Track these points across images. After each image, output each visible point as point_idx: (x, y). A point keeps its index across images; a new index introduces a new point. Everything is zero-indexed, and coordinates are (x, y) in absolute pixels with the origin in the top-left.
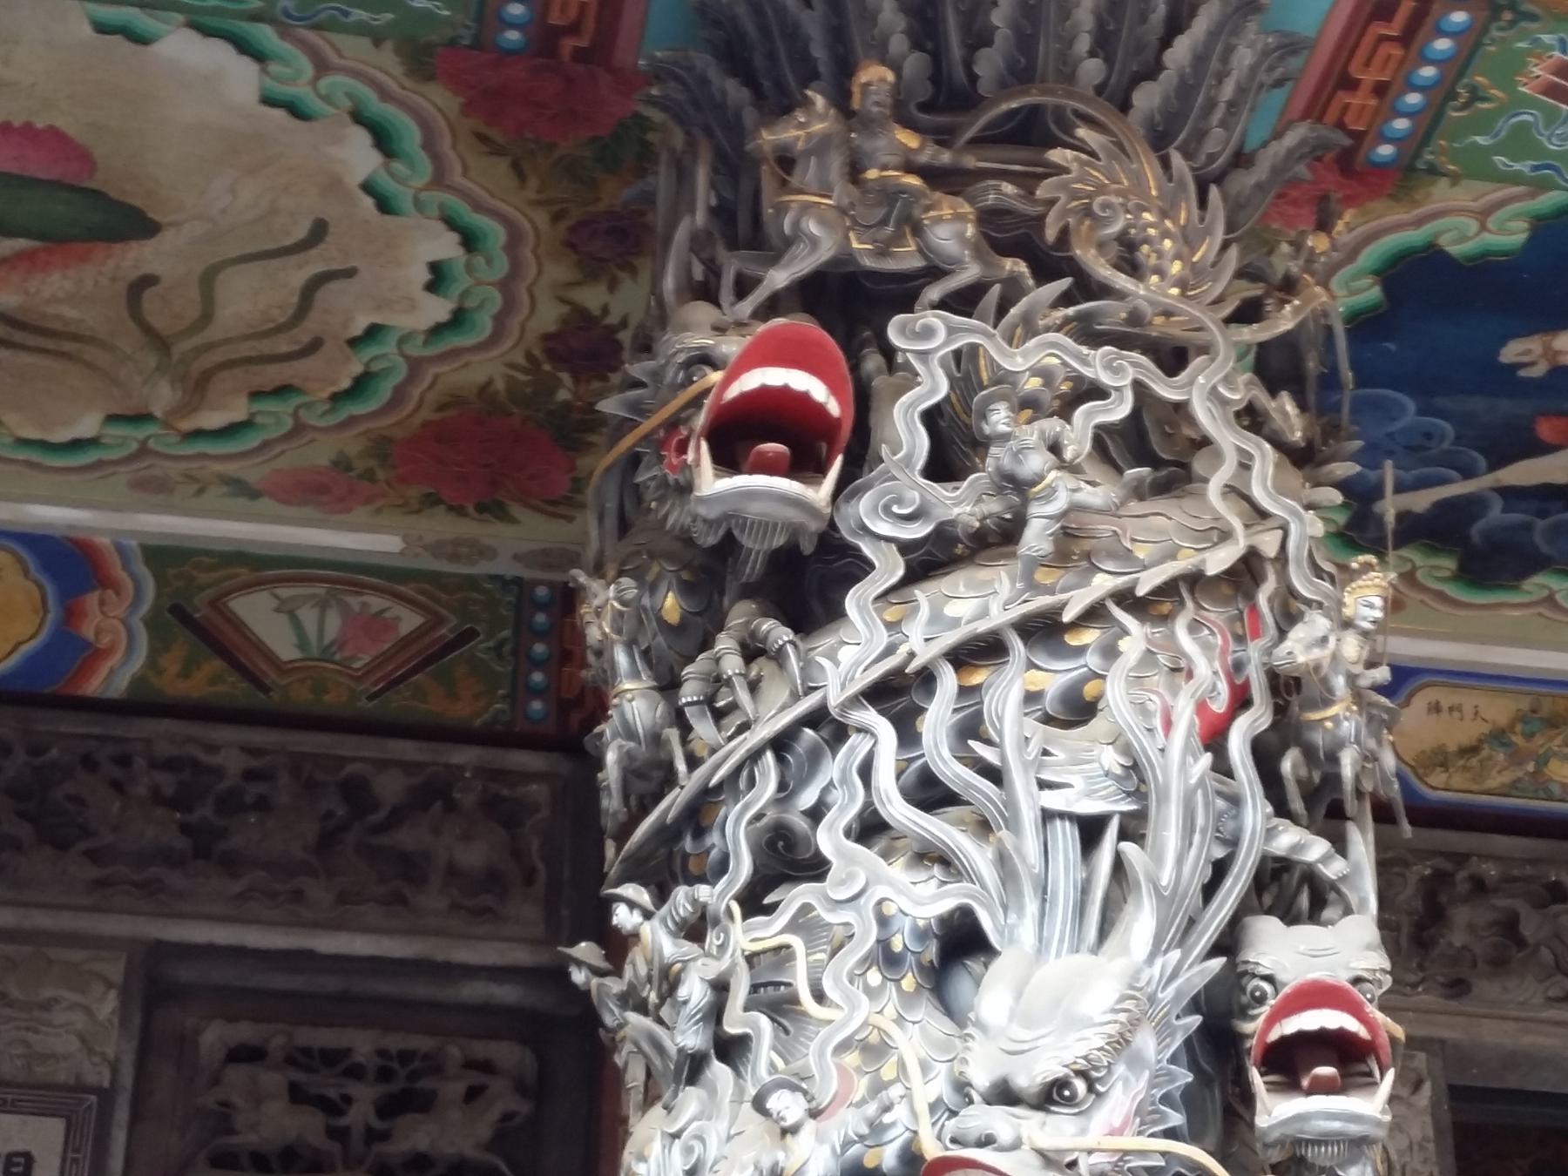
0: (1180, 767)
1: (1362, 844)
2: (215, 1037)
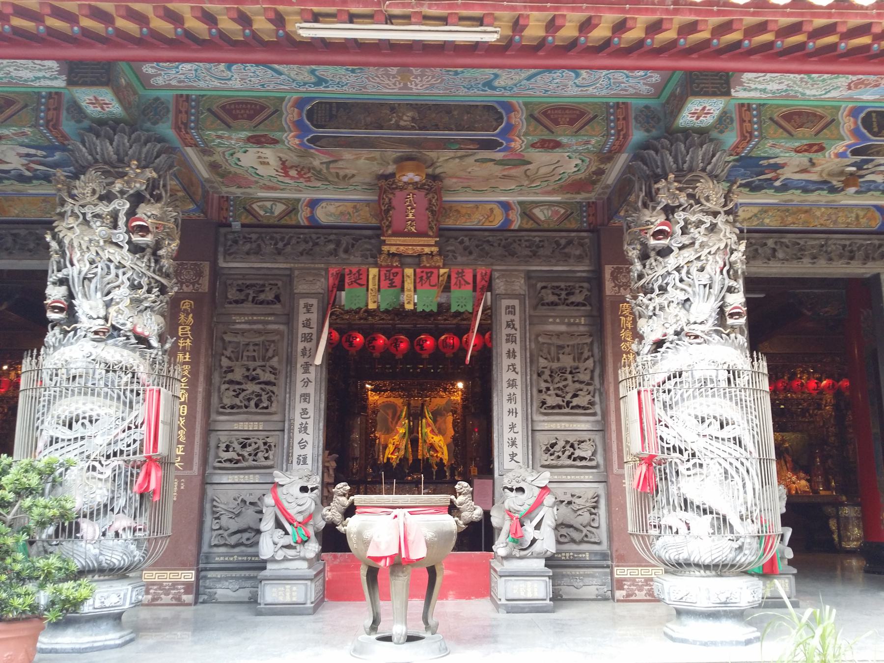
0: (718, 278)
1: (741, 281)
2: (539, 285)
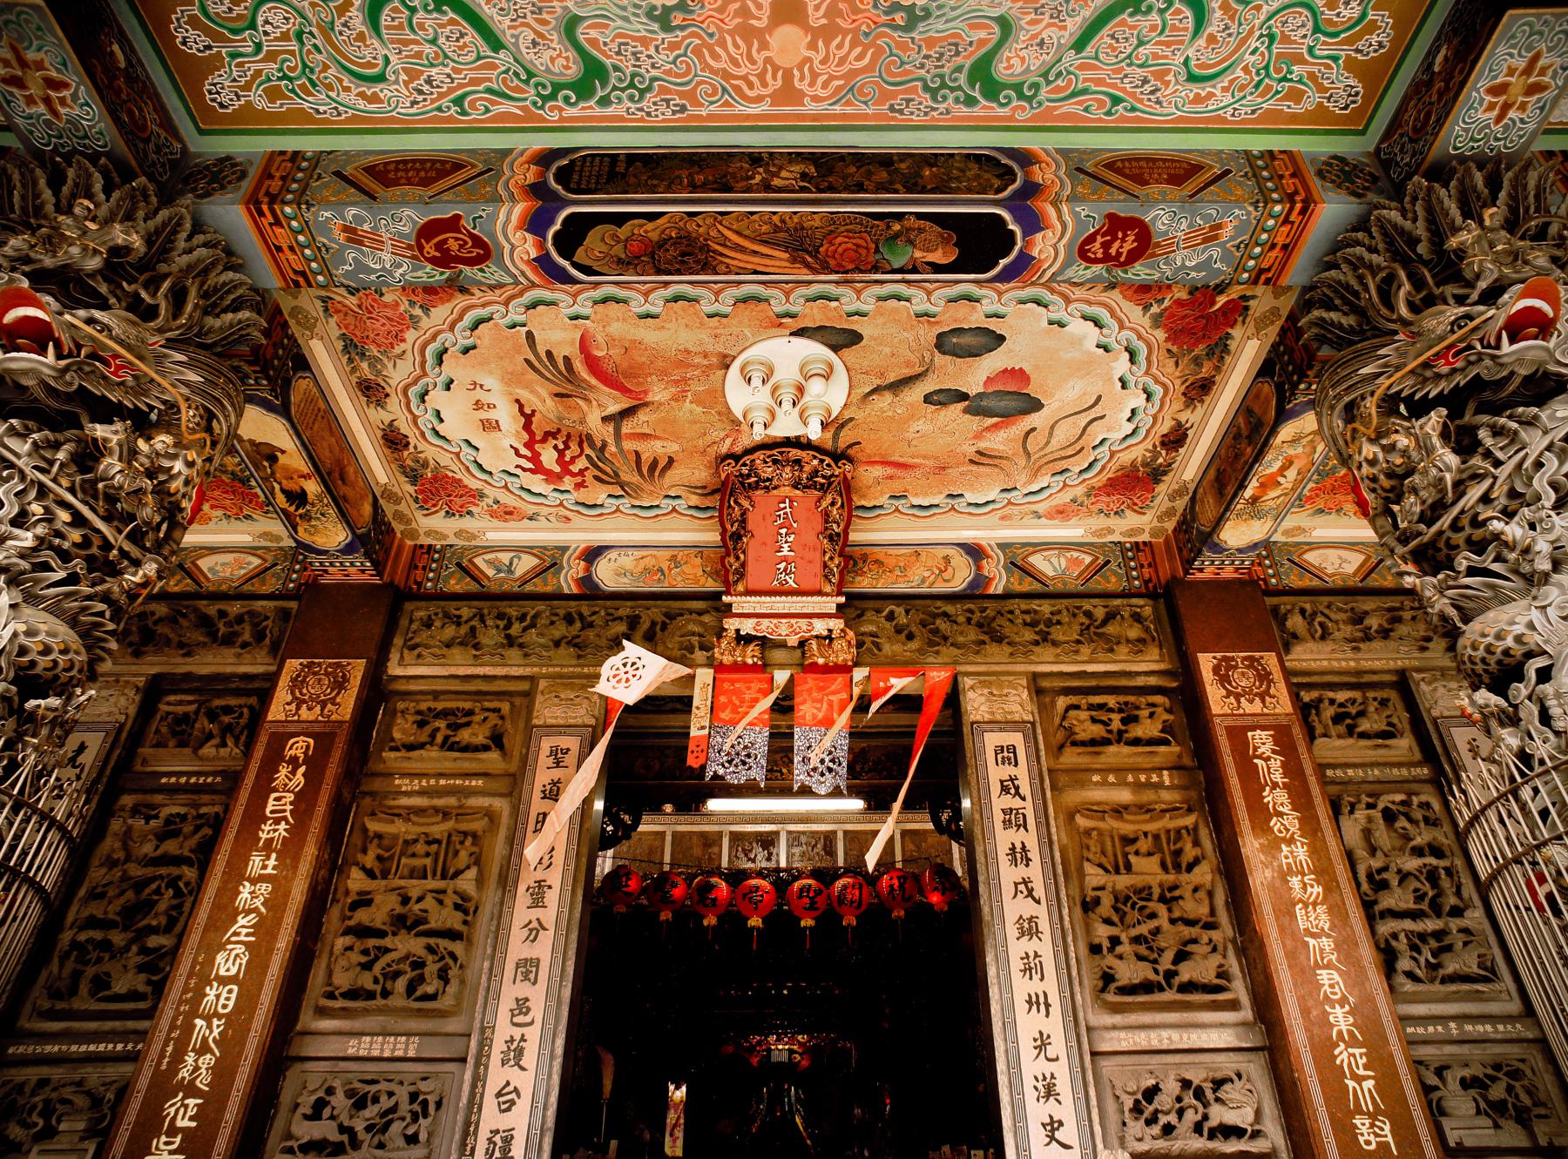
2: (1062, 702)
